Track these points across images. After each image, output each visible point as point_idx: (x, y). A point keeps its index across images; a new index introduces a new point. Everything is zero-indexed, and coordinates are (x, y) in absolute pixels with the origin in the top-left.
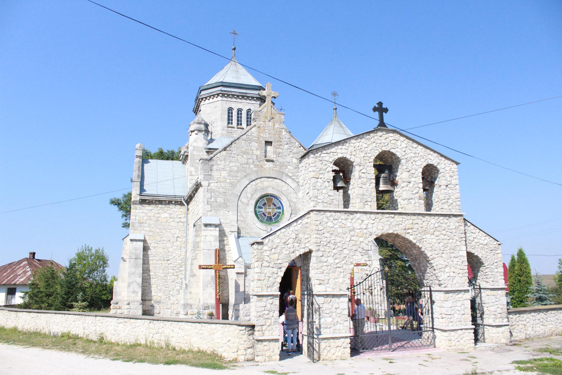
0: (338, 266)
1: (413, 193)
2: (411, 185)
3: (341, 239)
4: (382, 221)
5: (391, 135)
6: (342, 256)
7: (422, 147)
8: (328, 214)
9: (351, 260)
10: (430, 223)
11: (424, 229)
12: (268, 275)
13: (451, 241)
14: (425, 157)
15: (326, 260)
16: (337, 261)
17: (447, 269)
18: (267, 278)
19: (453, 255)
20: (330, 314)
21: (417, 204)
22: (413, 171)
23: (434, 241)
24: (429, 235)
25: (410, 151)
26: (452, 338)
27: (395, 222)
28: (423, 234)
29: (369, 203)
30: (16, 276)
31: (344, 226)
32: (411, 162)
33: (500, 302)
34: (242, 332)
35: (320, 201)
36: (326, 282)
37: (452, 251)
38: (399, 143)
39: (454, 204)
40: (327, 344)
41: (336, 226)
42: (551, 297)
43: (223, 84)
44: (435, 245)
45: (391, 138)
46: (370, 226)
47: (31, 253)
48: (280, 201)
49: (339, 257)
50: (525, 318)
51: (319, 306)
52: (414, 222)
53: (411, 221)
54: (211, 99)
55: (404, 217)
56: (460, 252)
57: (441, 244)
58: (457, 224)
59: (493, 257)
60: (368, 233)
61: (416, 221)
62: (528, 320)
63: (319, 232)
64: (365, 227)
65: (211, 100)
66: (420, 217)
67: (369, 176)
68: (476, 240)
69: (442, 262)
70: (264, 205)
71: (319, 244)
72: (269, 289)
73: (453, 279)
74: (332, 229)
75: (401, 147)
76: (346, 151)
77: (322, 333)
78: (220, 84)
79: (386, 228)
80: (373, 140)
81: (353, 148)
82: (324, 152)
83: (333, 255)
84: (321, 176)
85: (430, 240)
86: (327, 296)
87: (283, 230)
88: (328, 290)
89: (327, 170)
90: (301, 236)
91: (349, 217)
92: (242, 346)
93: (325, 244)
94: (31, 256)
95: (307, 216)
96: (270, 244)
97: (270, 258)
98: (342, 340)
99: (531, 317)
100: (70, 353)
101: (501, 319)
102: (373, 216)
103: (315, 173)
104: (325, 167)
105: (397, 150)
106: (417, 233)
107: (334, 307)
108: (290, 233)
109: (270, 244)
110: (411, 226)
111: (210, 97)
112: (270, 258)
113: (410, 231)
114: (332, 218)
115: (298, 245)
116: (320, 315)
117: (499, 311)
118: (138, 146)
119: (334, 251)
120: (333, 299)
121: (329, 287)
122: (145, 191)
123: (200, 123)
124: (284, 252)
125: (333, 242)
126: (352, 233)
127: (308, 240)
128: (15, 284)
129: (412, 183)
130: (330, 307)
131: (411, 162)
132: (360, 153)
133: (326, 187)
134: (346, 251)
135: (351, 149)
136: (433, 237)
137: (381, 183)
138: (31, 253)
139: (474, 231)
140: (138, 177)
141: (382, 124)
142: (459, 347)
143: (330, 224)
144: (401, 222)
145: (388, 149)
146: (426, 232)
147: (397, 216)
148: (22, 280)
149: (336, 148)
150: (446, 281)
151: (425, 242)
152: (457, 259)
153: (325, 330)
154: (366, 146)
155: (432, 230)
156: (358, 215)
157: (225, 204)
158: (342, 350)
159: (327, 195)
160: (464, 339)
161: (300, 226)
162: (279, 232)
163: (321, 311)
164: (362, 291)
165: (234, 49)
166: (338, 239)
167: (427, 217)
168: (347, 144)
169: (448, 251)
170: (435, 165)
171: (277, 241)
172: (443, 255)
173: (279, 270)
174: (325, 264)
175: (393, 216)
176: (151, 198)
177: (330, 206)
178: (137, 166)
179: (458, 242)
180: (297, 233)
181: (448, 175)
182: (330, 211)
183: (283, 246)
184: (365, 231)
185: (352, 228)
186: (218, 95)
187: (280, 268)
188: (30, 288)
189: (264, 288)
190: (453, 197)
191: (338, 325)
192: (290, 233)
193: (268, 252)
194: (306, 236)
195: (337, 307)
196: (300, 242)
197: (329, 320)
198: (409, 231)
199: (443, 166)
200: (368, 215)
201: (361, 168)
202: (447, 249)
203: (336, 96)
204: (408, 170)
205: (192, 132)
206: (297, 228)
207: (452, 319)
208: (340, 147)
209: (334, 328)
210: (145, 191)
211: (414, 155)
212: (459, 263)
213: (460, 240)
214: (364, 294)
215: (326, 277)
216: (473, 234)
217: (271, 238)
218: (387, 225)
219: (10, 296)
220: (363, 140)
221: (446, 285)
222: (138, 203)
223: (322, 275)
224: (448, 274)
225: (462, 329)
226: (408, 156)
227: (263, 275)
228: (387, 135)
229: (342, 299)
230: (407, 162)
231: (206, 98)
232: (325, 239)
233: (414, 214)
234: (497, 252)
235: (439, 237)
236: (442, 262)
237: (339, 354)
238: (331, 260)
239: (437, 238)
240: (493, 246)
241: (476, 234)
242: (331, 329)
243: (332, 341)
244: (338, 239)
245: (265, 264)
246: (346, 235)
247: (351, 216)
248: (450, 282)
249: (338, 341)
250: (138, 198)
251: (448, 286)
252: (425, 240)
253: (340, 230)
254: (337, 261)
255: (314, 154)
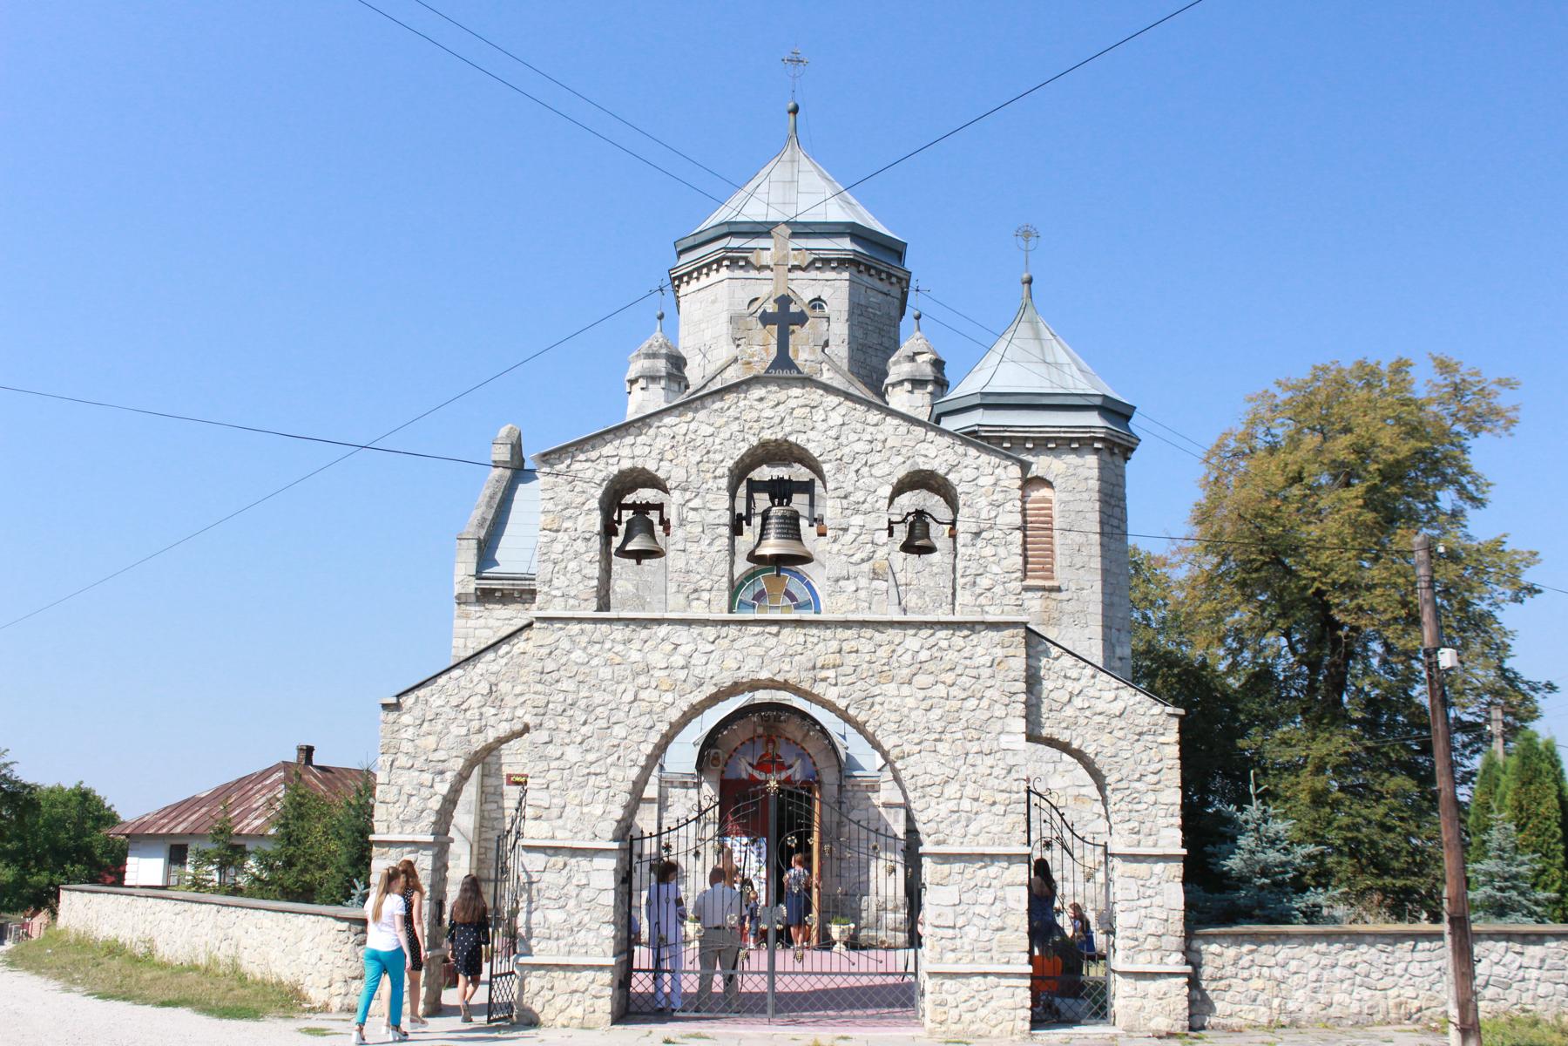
0: (592, 770)
1: (853, 559)
2: (849, 537)
3: (608, 697)
4: (737, 645)
5: (796, 391)
6: (607, 743)
7: (896, 422)
8: (575, 628)
9: (634, 756)
10: (900, 650)
11: (877, 667)
12: (407, 789)
13: (972, 703)
14: (904, 451)
15: (558, 754)
16: (591, 757)
17: (952, 790)
18: (404, 798)
19: (974, 747)
20: (561, 903)
21: (862, 594)
22: (859, 496)
23: (911, 702)
24: (893, 685)
25: (853, 437)
26: (950, 998)
27: (782, 649)
28: (873, 681)
29: (705, 596)
30: (250, 811)
31: (618, 660)
32: (854, 468)
33: (1157, 900)
34: (343, 936)
35: (558, 593)
36: (555, 812)
37: (975, 734)
38: (819, 415)
39: (998, 589)
40: (545, 982)
41: (594, 662)
42: (1537, 903)
43: (734, 229)
44: (913, 714)
45: (792, 403)
46: (698, 659)
47: (300, 749)
48: (809, 585)
49: (597, 745)
50: (1280, 957)
51: (529, 876)
52: (846, 647)
53: (834, 645)
54: (703, 278)
55: (814, 631)
56: (1003, 738)
57: (935, 714)
58: (999, 652)
59: (1145, 756)
60: (692, 680)
61: (853, 643)
62: (1293, 965)
63: (545, 677)
64: (682, 662)
65: (704, 281)
66: (868, 632)
67: (711, 518)
68: (1078, 702)
69: (933, 767)
70: (760, 596)
71: (541, 711)
72: (408, 828)
73: (969, 821)
74: (582, 669)
75: (825, 426)
76: (647, 449)
77: (535, 950)
78: (725, 229)
79: (752, 663)
80: (732, 412)
81: (667, 440)
82: (582, 457)
83: (579, 739)
84: (565, 525)
85: (897, 700)
86: (557, 850)
87: (456, 673)
88: (559, 834)
89: (586, 507)
90: (504, 687)
91: (635, 636)
92: (340, 971)
93: (560, 710)
94: (303, 756)
95: (525, 635)
96: (417, 712)
97: (416, 747)
98: (590, 974)
99: (1314, 959)
100: (36, 978)
101: (1156, 956)
102: (711, 632)
103: (551, 516)
104: (581, 500)
105: (811, 434)
106: (852, 679)
107: (575, 881)
108: (476, 680)
109: (417, 712)
110: (831, 659)
111: (699, 270)
112: (416, 747)
113: (831, 673)
114: (585, 639)
115: (493, 711)
116: (530, 901)
117: (1151, 926)
118: (503, 431)
119: (584, 730)
120: (573, 861)
121: (563, 828)
122: (496, 563)
123: (654, 356)
124: (454, 730)
125: (582, 704)
126: (642, 680)
127: (521, 699)
128: (238, 835)
129: (853, 530)
130: (563, 881)
131: (854, 468)
132: (690, 453)
133: (577, 555)
134: (619, 731)
135: (660, 443)
136: (905, 690)
137: (772, 533)
138: (300, 749)
139: (1074, 673)
140: (481, 525)
141: (783, 360)
142: (973, 1027)
143: (578, 655)
144: (799, 649)
145: (779, 436)
146: (884, 675)
147: (786, 631)
148: (258, 822)
149: (616, 443)
150: (942, 826)
151: (877, 707)
152: (989, 761)
153: (543, 945)
154: (710, 430)
155: (906, 672)
156: (663, 630)
157: (638, 597)
158: (588, 1003)
159: (578, 577)
160: (993, 1004)
161: (504, 660)
162: (445, 678)
163: (534, 893)
164: (691, 846)
165: (795, 111)
166: (598, 698)
167: (890, 631)
168: (652, 431)
169: (959, 735)
170: (941, 472)
171: (437, 701)
172: (940, 746)
173: (438, 779)
174: (554, 764)
175: (774, 629)
176: (506, 585)
177: (584, 605)
178: (488, 492)
179: (997, 706)
180: (493, 679)
181: (983, 502)
182: (580, 620)
183: (453, 715)
184: (682, 675)
185: (642, 665)
186: (719, 262)
187: (442, 773)
188: (215, 841)
189: (395, 823)
190: (995, 569)
191: (583, 932)
192: (476, 680)
193: (411, 730)
194: (518, 690)
195: (584, 881)
196: (500, 704)
197: (556, 917)
198: (824, 674)
199: (969, 473)
200: (695, 630)
201: (688, 495)
202: (953, 728)
203: (1033, 240)
204: (841, 493)
205: (633, 382)
206: (494, 667)
207: (958, 942)
208: (629, 440)
209: (570, 940)
210: (496, 563)
211: (868, 448)
212: (996, 771)
213: (1007, 700)
214: (697, 854)
215: (555, 801)
216: (1068, 683)
217: (421, 693)
218: (763, 657)
219: (175, 868)
220: (702, 415)
221: (941, 837)
222: (473, 599)
223: (544, 794)
224: (952, 805)
225: (985, 975)
226: (846, 450)
227: (395, 790)
228: (782, 395)
229: (599, 862)
230: (839, 470)
231: (689, 274)
232: (561, 697)
233: (846, 624)
234: (1161, 739)
235: (929, 693)
236: (933, 767)
237: (578, 1012)
238: (573, 754)
239: (921, 694)
240: (1147, 719)
241: (1083, 682)
242: (562, 943)
243: (559, 974)
244: (598, 698)
245: (403, 761)
246: (622, 687)
247: (644, 633)
248: (958, 830)
249: (576, 975)
250: (472, 586)
251: (951, 841)
252: (878, 699)
253: (605, 673)
254: (591, 757)
255: (552, 466)
